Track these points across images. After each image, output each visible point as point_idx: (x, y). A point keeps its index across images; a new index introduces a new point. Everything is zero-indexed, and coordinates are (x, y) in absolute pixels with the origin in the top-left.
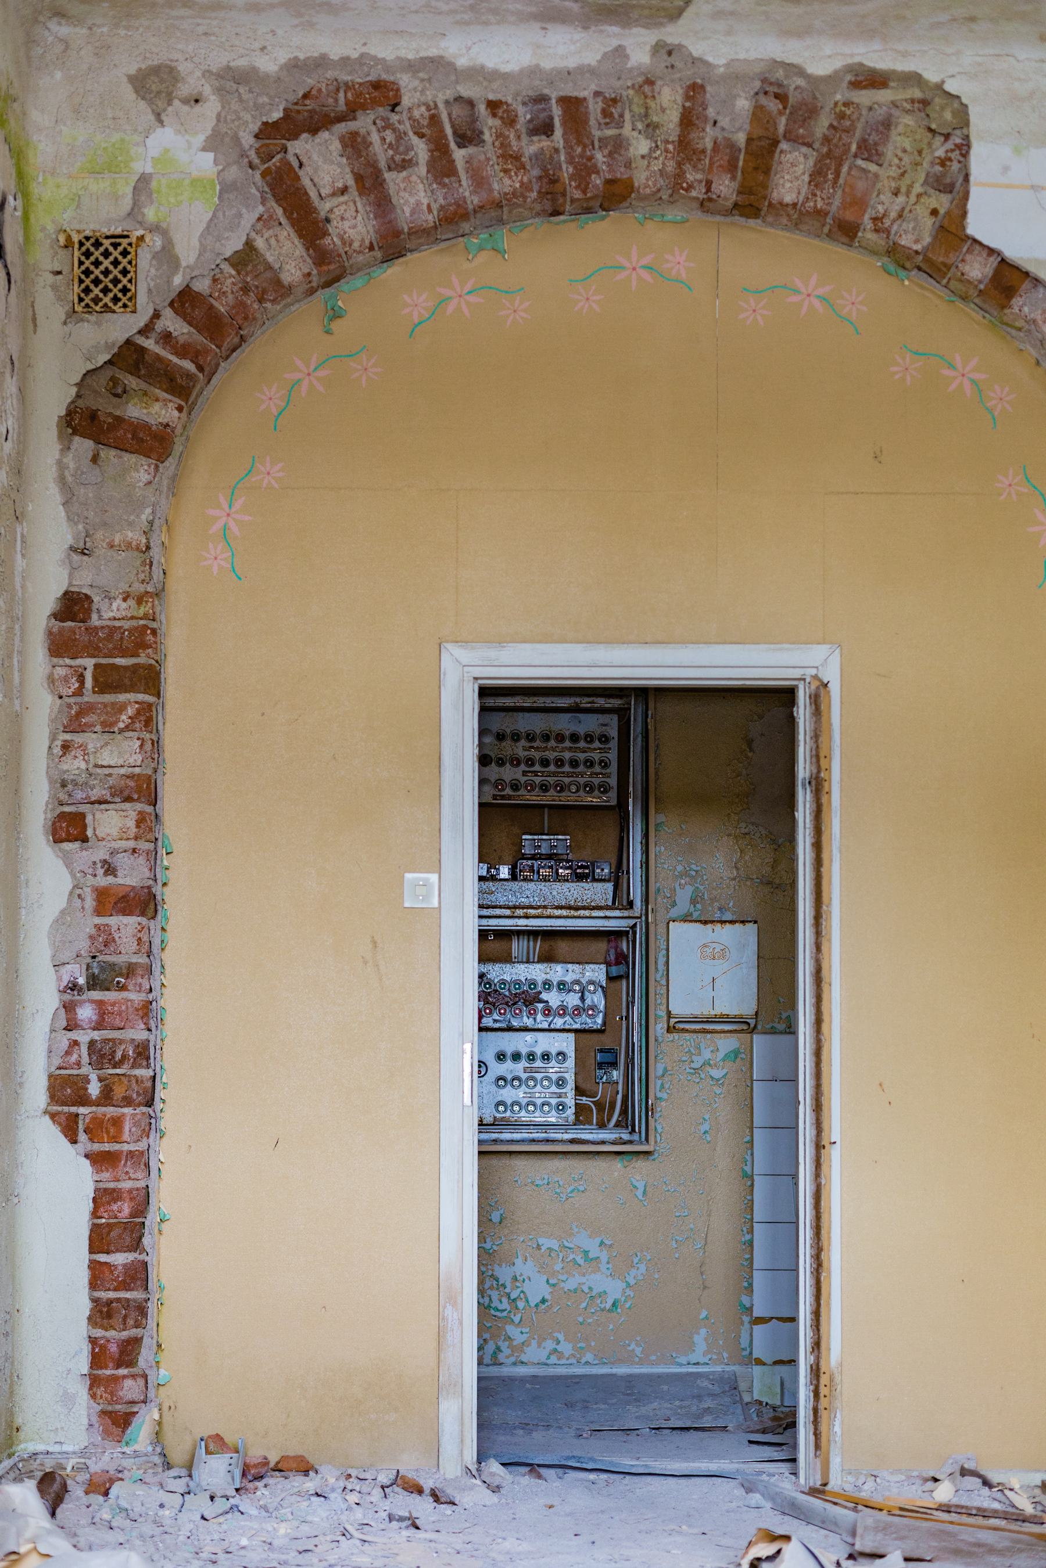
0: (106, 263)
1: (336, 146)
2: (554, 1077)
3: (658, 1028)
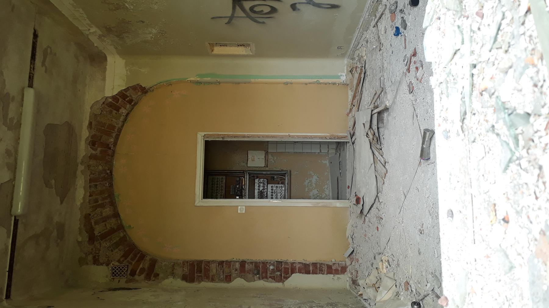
0: (117, 271)
1: (97, 226)
2: (276, 188)
3: (267, 169)
